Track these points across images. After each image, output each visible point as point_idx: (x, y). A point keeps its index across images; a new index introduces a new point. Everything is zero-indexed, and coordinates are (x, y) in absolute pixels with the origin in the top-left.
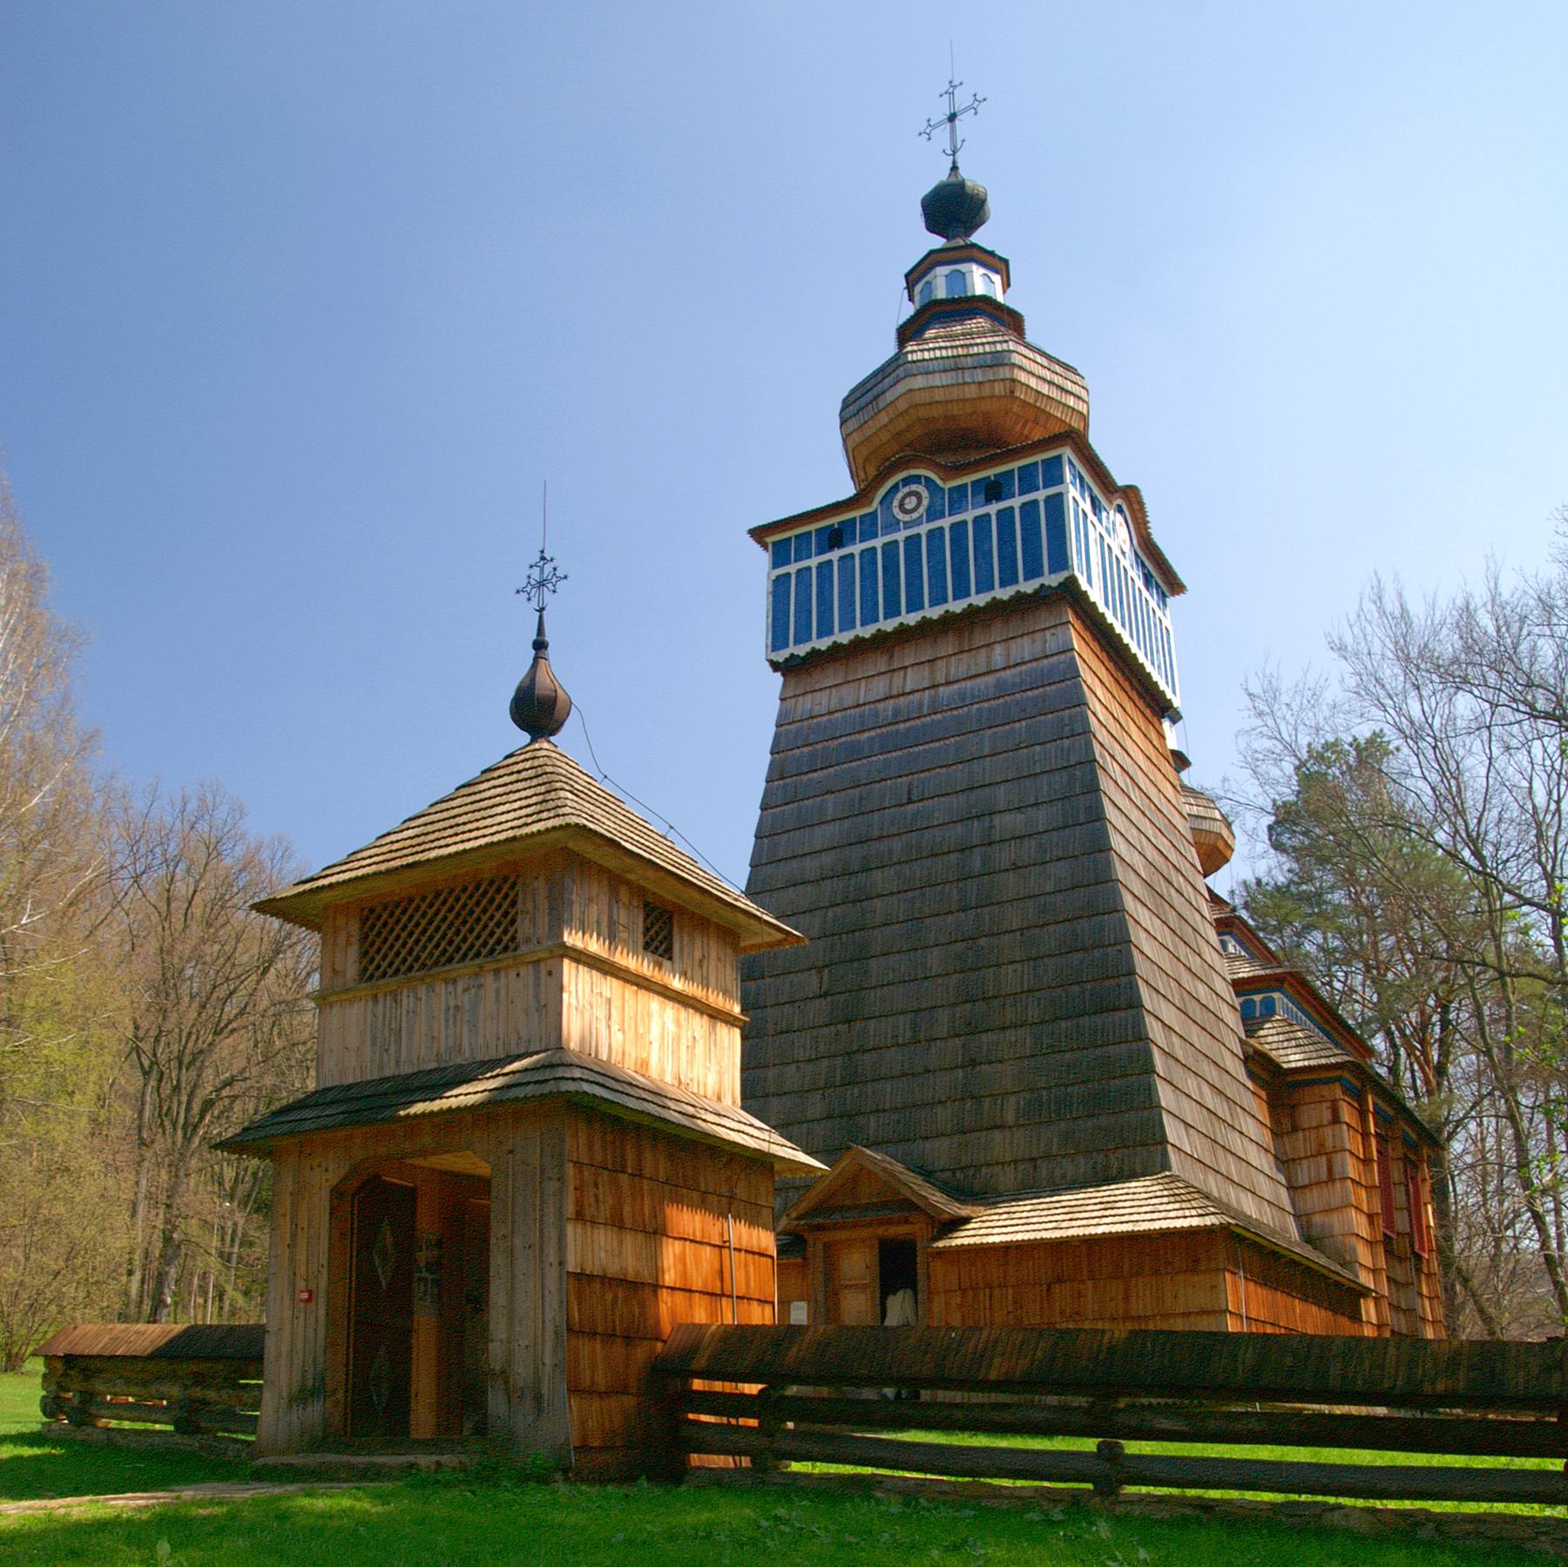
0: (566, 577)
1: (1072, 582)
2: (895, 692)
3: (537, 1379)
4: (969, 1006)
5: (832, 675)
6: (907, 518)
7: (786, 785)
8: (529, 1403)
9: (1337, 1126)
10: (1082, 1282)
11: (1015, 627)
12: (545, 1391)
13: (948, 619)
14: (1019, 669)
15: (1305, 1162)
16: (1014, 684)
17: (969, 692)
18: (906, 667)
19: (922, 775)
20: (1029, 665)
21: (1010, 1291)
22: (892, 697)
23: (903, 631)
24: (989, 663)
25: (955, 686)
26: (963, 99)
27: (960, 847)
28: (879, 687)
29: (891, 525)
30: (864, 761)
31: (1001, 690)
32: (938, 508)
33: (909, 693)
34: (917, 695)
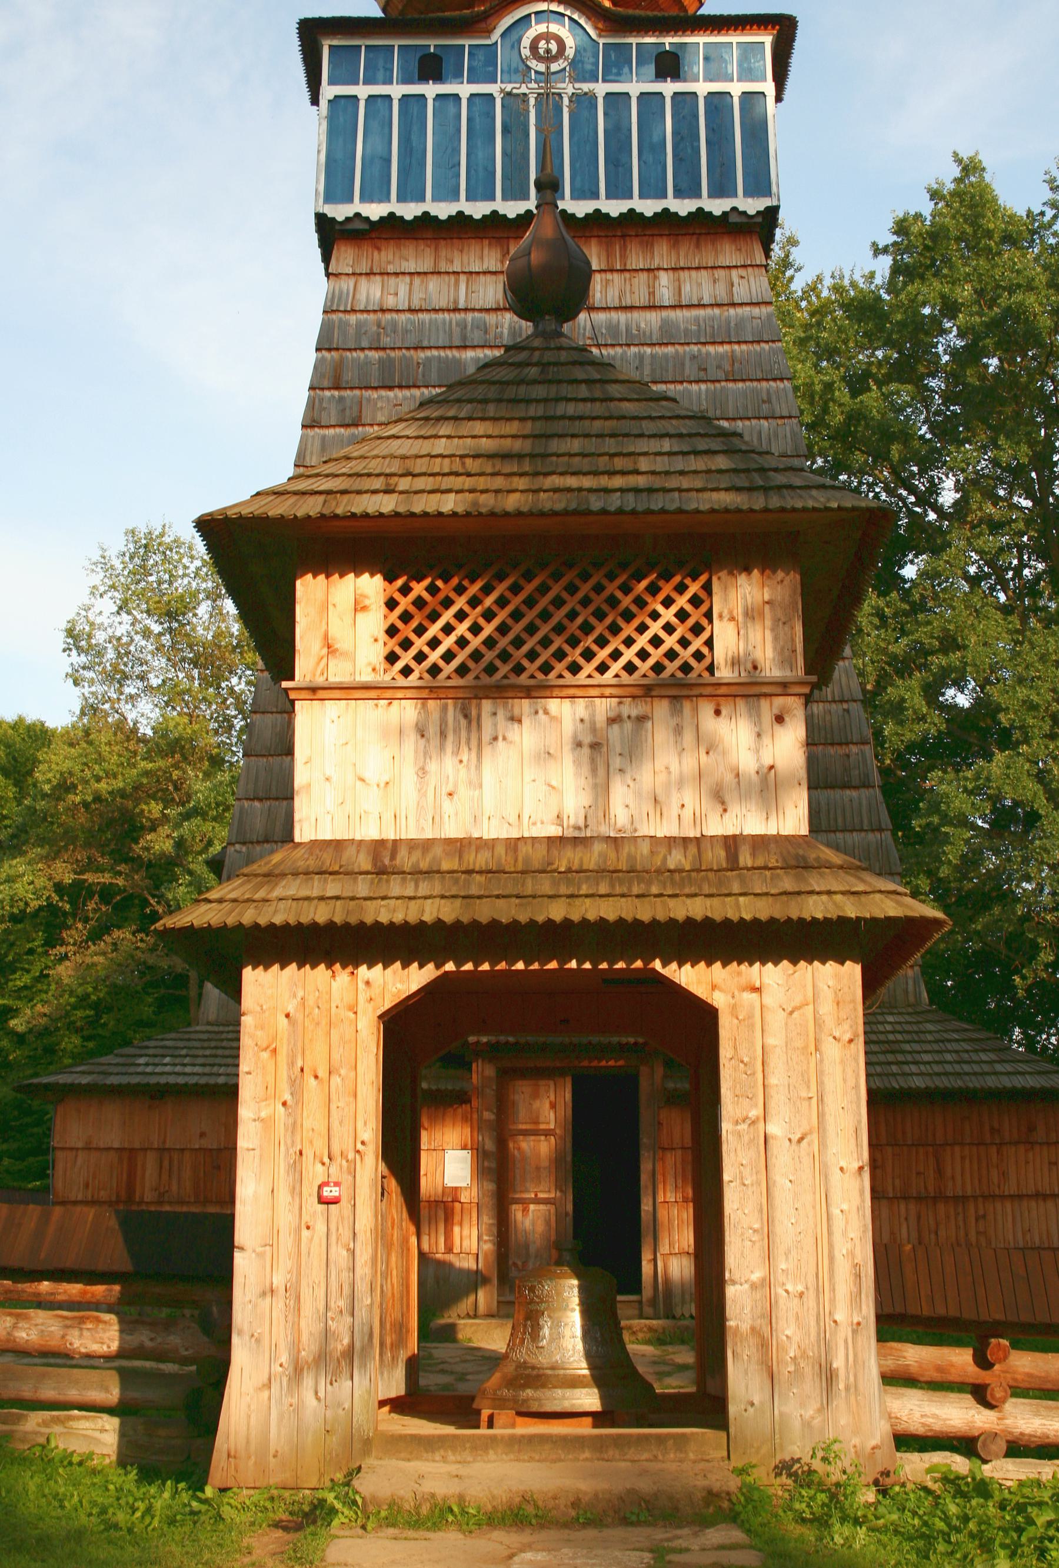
3: (826, 1344)
7: (341, 399)
8: (811, 1386)
11: (686, 255)
12: (838, 1363)
14: (695, 312)
17: (623, 328)
20: (709, 311)
24: (652, 294)
31: (667, 337)
32: (588, 67)
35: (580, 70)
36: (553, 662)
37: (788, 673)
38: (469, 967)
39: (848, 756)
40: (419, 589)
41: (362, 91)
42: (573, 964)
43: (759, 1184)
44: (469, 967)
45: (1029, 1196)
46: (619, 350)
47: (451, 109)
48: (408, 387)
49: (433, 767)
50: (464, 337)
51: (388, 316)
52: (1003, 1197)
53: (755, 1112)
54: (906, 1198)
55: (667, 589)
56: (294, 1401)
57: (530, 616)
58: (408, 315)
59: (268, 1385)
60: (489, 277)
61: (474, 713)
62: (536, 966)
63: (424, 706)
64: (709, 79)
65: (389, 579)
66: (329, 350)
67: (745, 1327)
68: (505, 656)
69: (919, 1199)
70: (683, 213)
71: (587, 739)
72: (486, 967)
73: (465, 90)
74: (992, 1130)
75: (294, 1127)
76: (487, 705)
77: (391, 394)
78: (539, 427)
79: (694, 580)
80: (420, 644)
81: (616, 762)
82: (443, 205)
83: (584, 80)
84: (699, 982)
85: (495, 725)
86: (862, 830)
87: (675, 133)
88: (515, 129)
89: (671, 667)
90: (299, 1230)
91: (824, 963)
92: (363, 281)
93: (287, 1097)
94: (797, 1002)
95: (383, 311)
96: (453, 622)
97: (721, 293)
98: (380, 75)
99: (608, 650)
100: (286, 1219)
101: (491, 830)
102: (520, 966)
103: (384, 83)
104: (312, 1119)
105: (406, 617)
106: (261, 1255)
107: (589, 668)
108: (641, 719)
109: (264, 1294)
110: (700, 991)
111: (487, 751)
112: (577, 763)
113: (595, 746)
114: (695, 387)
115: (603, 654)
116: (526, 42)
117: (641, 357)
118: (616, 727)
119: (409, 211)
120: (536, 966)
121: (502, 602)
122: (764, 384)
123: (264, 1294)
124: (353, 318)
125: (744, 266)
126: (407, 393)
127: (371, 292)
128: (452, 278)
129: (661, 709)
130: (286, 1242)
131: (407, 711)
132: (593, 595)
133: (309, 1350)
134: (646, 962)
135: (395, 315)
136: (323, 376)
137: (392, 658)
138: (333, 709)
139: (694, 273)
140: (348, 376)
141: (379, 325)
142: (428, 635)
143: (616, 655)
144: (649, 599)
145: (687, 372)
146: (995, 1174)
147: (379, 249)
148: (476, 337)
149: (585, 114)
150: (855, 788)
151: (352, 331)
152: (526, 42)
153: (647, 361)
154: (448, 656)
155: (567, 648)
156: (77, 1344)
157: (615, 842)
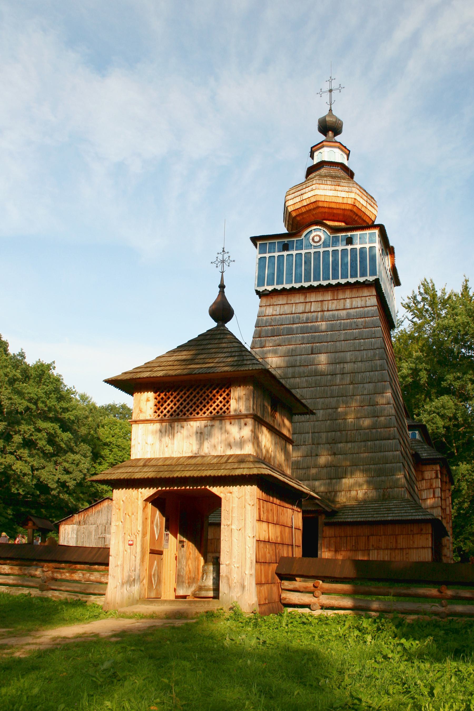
0: (234, 261)
1: (377, 281)
2: (307, 311)
4: (334, 433)
5: (281, 300)
6: (315, 244)
7: (261, 340)
9: (437, 479)
10: (380, 536)
11: (355, 293)
13: (329, 286)
15: (426, 491)
16: (353, 315)
17: (336, 315)
18: (311, 302)
19: (317, 344)
20: (360, 309)
21: (354, 538)
22: (305, 312)
23: (311, 287)
24: (344, 305)
25: (331, 313)
26: (335, 85)
27: (331, 373)
28: (301, 308)
29: (308, 246)
30: (294, 336)
31: (348, 317)
32: (328, 243)
33: (312, 312)
34: (316, 314)
35: (325, 244)
36: (193, 412)
37: (248, 413)
38: (164, 488)
39: (390, 431)
40: (162, 395)
41: (267, 255)
42: (188, 487)
43: (229, 540)
44: (164, 488)
45: (420, 548)
46: (335, 322)
47: (291, 258)
48: (278, 336)
49: (163, 439)
50: (293, 321)
51: (274, 317)
52: (413, 548)
53: (229, 523)
54: (387, 549)
55: (221, 392)
56: (122, 591)
57: (188, 400)
58: (279, 316)
59: (116, 587)
60: (301, 304)
61: (173, 426)
62: (179, 488)
63: (162, 425)
64: (360, 244)
65: (155, 392)
66: (258, 327)
67: (224, 575)
68: (181, 411)
69: (391, 549)
70: (352, 282)
71: (199, 431)
72: (168, 488)
73: (294, 252)
74: (411, 530)
75: (124, 527)
76: (176, 424)
77: (274, 338)
78: (197, 352)
79: (175, 392)
80: (162, 409)
81: (206, 437)
82: (288, 285)
83: (327, 247)
84: (218, 491)
85: (178, 429)
86: (392, 451)
87: (351, 260)
88: (308, 262)
89: (221, 412)
90: (124, 552)
91: (247, 486)
92: (268, 307)
93: (122, 520)
94: (240, 496)
95: (273, 315)
96: (170, 403)
97: (363, 304)
98: (272, 250)
99: (206, 408)
100: (121, 549)
101: (176, 455)
102: (176, 488)
103: (274, 252)
104: (128, 526)
105: (159, 402)
106: (115, 557)
107: (201, 413)
108: (212, 426)
109: (116, 567)
110: (217, 493)
111: (176, 435)
112: (197, 438)
113: (201, 433)
114: (355, 331)
115: (204, 409)
116: (311, 238)
117: (341, 323)
118: (206, 428)
119: (279, 287)
120: (179, 488)
121: (181, 397)
122: (374, 329)
123: (116, 567)
124: (265, 318)
125: (370, 296)
126: (278, 337)
127: (269, 311)
128: (291, 305)
129: (217, 423)
130: (121, 554)
131: (157, 426)
132: (197, 395)
133: (126, 579)
134: (205, 487)
135: (276, 316)
136: (256, 334)
137: (156, 412)
138: (141, 426)
139: (356, 299)
140: (263, 334)
141: (271, 319)
142: (164, 406)
143: (208, 409)
144: (216, 394)
145: (353, 326)
146: (411, 542)
147: (272, 298)
148: (297, 321)
149: (327, 256)
150: (392, 439)
151: (264, 322)
152: (311, 238)
153: (342, 324)
154: (168, 412)
155: (196, 408)
156: (103, 580)
157: (203, 457)
